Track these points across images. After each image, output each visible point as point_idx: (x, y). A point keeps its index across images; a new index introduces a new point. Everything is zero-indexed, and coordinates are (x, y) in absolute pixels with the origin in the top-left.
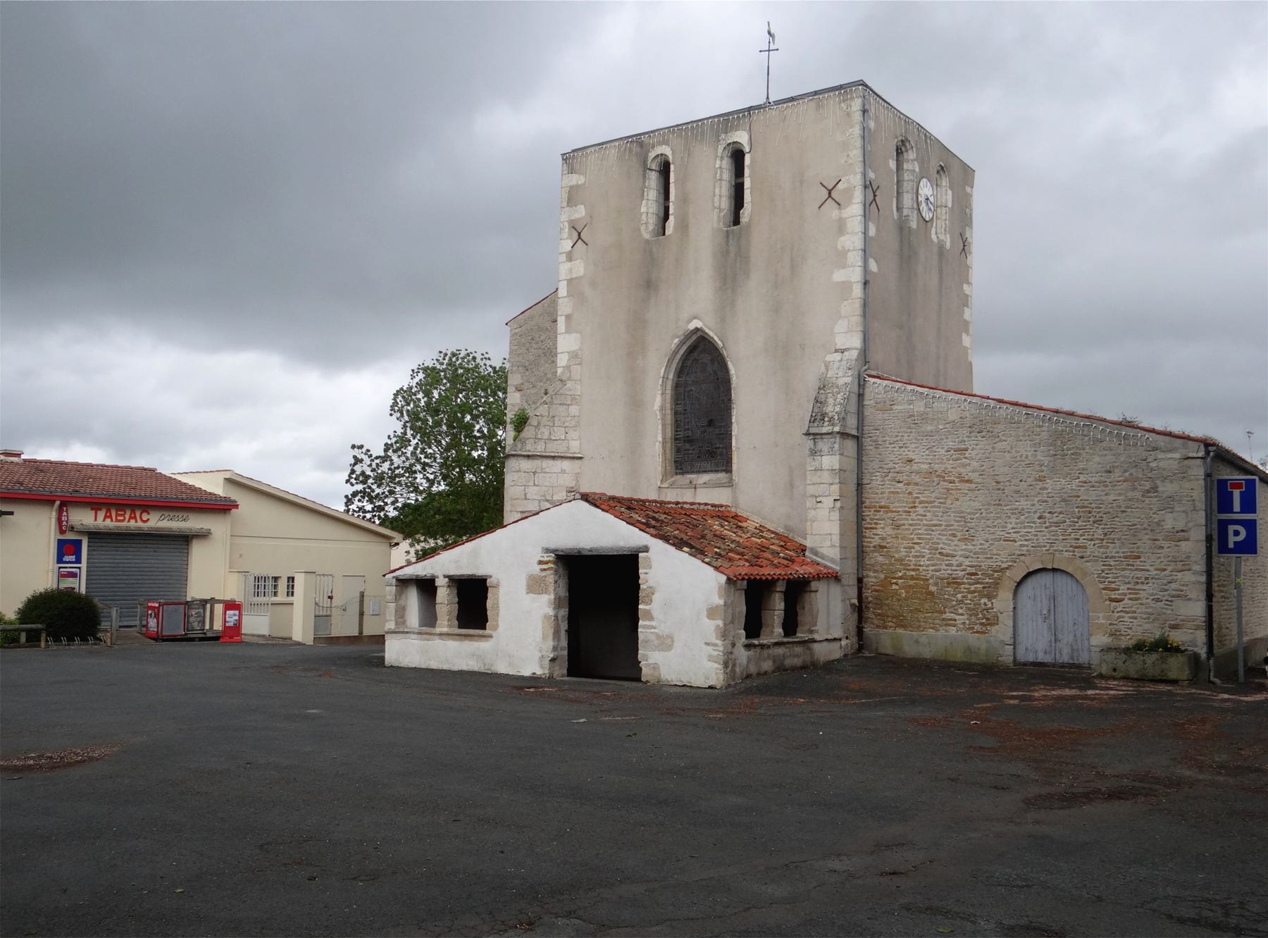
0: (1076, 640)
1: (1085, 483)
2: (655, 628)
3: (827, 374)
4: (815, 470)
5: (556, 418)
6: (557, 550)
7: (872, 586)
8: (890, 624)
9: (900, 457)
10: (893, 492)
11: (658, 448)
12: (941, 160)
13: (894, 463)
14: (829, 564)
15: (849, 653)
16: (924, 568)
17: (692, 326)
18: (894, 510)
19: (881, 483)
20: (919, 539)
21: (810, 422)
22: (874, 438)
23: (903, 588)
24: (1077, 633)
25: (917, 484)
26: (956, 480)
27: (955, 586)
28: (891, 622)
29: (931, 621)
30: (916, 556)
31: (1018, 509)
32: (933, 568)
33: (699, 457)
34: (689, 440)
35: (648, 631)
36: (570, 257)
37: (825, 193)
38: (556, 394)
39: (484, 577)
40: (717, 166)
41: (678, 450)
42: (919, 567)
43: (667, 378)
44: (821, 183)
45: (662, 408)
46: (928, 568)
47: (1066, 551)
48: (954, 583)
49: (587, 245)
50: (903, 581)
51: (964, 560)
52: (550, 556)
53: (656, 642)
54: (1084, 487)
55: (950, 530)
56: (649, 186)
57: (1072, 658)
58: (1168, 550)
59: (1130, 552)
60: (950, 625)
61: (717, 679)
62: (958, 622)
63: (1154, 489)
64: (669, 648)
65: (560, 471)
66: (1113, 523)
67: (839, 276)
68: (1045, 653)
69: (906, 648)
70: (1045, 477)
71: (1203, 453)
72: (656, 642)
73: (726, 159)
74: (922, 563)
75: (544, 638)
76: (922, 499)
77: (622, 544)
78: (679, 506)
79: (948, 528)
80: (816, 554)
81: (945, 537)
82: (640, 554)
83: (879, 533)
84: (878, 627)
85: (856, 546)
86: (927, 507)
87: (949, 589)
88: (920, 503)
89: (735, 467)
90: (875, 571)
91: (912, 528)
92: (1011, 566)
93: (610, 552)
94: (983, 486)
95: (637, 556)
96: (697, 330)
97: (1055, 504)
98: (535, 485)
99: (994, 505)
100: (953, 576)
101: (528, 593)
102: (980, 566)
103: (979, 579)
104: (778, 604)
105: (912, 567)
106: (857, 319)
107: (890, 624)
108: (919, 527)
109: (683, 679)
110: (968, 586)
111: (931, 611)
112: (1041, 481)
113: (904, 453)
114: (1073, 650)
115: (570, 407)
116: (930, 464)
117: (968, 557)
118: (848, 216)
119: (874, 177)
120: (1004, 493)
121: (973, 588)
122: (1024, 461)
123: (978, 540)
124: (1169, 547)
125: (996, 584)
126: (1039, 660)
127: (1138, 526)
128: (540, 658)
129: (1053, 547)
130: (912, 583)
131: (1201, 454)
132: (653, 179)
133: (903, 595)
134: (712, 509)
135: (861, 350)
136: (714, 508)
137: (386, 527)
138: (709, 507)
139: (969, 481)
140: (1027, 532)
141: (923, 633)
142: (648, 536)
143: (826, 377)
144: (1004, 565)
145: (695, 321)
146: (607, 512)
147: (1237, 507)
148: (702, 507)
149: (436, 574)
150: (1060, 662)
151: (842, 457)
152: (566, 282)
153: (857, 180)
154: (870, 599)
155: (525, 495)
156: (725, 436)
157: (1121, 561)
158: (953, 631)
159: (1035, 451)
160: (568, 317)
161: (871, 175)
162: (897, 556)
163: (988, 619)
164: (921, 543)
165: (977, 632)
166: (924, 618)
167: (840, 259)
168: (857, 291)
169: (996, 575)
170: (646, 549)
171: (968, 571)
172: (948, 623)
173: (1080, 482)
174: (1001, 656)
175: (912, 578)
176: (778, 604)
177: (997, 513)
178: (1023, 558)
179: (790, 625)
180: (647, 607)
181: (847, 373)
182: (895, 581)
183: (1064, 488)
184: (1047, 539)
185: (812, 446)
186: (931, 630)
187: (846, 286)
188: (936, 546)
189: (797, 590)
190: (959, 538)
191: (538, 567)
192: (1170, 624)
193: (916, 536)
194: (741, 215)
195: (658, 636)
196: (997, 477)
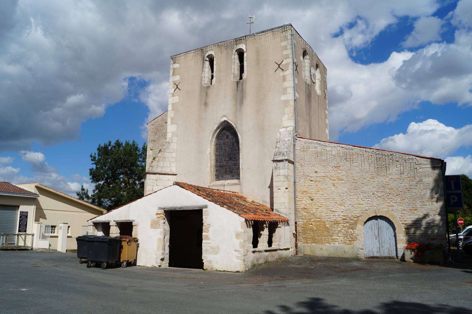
0: (391, 246)
1: (392, 179)
2: (210, 244)
3: (280, 137)
4: (277, 176)
5: (166, 158)
6: (165, 208)
7: (301, 225)
8: (309, 241)
9: (312, 170)
10: (309, 185)
11: (208, 169)
12: (317, 62)
13: (309, 173)
14: (284, 216)
15: (293, 254)
16: (324, 217)
17: (223, 120)
18: (310, 192)
19: (304, 182)
20: (321, 205)
21: (274, 156)
22: (300, 163)
23: (315, 226)
24: (391, 244)
25: (319, 182)
26: (336, 179)
27: (337, 224)
28: (310, 241)
29: (327, 240)
30: (320, 212)
31: (363, 191)
32: (327, 217)
33: (225, 173)
34: (221, 166)
35: (207, 245)
36: (173, 95)
37: (277, 66)
38: (166, 148)
39: (131, 221)
40: (233, 57)
41: (217, 171)
42: (322, 217)
43: (212, 141)
44: (275, 62)
45: (210, 153)
46: (325, 217)
47: (385, 208)
48: (337, 223)
49: (180, 90)
50: (314, 223)
51: (341, 213)
52: (161, 211)
53: (211, 251)
54: (391, 180)
55: (335, 200)
56: (205, 66)
57: (389, 254)
58: (429, 206)
59: (413, 207)
60: (336, 241)
61: (241, 268)
62: (339, 240)
63: (421, 181)
64: (217, 253)
65: (167, 179)
66: (405, 195)
67: (283, 98)
68: (377, 252)
69: (317, 252)
70: (374, 177)
71: (441, 165)
72: (211, 251)
73: (236, 55)
74: (323, 215)
75: (158, 249)
76: (322, 188)
77: (195, 205)
78: (219, 191)
79: (334, 200)
80: (278, 211)
81: (332, 204)
82: (203, 209)
83: (303, 203)
84: (304, 243)
85: (294, 208)
86: (324, 191)
87: (335, 226)
88: (321, 190)
89: (241, 176)
90: (302, 219)
91: (318, 200)
92: (361, 215)
93: (189, 208)
94: (348, 182)
95: (202, 210)
96: (225, 121)
97: (379, 188)
98: (157, 185)
99: (353, 189)
100: (336, 220)
101: (151, 228)
102: (348, 216)
103: (348, 221)
104: (265, 233)
105: (318, 217)
106: (292, 114)
107: (309, 241)
108: (321, 200)
109: (223, 268)
110: (343, 224)
111: (327, 235)
112: (373, 178)
113: (314, 169)
114: (389, 250)
115: (172, 153)
116: (325, 173)
117: (342, 212)
118: (287, 74)
119: (296, 61)
120: (357, 184)
121: (345, 225)
122: (365, 170)
123: (347, 204)
124: (429, 205)
125: (356, 223)
126: (375, 255)
127: (415, 196)
128: (156, 258)
129: (379, 206)
130: (318, 223)
131: (440, 165)
132: (207, 64)
133: (315, 229)
134: (232, 193)
135: (294, 127)
136: (233, 193)
137: (95, 205)
138: (231, 193)
139: (342, 180)
140: (368, 200)
141: (324, 245)
142: (207, 201)
143: (280, 137)
144: (358, 215)
145: (224, 117)
146: (188, 190)
147: (453, 187)
148: (228, 192)
149: (110, 220)
150: (384, 256)
151: (288, 170)
152: (171, 105)
153: (290, 60)
154: (300, 231)
155: (153, 189)
156: (237, 165)
157: (409, 211)
158: (337, 244)
159: (370, 166)
160: (172, 118)
161: (295, 60)
162: (312, 212)
163: (352, 238)
164: (322, 207)
165: (348, 244)
166: (324, 239)
167: (284, 91)
168: (292, 103)
169: (355, 219)
170: (206, 207)
171: (343, 218)
172: (334, 240)
173: (389, 178)
174: (358, 254)
175: (319, 221)
176: (265, 233)
177: (354, 193)
178: (366, 211)
179: (270, 243)
180: (207, 234)
181: (289, 136)
182: (311, 223)
183: (383, 181)
184: (376, 203)
185: (276, 165)
186: (327, 244)
187: (287, 102)
188: (329, 207)
189: (273, 226)
190: (338, 204)
191: (156, 216)
192: (431, 238)
193: (320, 204)
194: (243, 76)
195: (212, 248)
196: (354, 178)
